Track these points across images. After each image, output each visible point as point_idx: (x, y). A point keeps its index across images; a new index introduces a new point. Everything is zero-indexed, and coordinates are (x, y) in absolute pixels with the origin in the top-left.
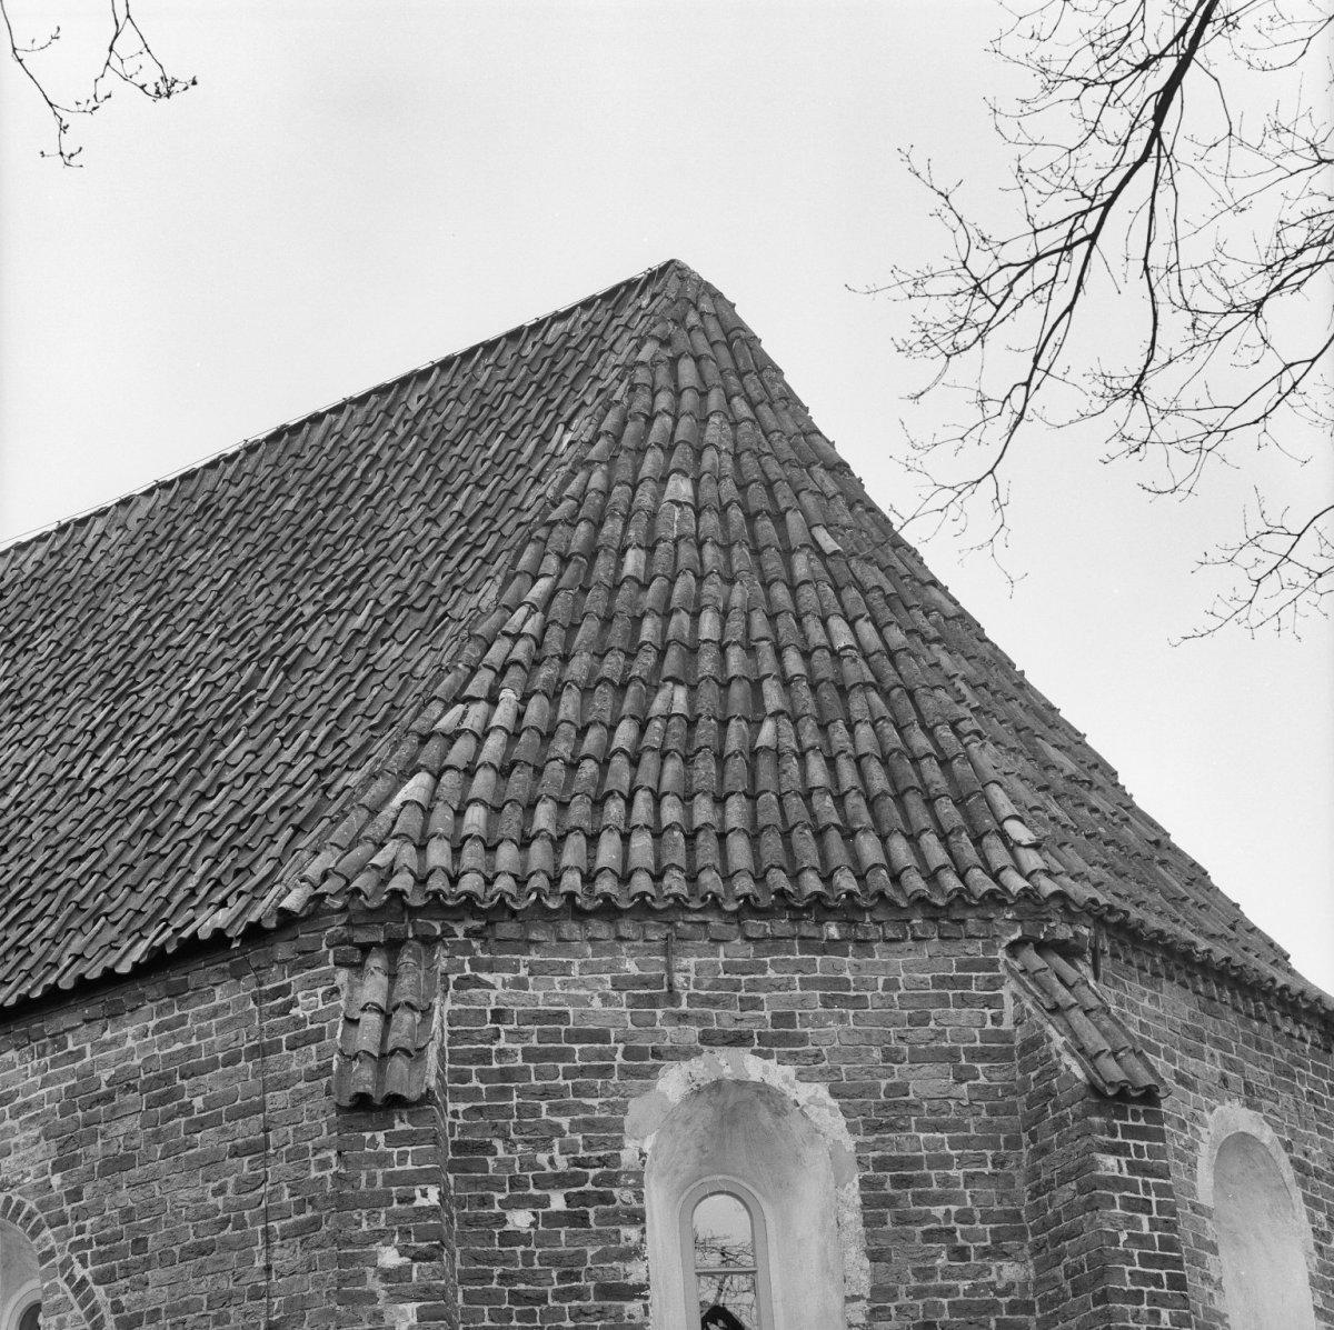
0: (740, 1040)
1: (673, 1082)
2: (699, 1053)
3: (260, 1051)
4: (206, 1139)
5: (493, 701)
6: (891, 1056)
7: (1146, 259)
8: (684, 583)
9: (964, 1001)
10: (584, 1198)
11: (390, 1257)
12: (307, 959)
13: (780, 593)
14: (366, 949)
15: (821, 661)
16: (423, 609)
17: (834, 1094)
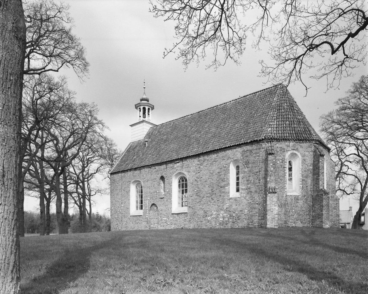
0: (294, 150)
1: (289, 153)
3: (259, 149)
4: (254, 155)
5: (274, 122)
6: (304, 151)
7: (61, 66)
8: (287, 113)
9: (310, 147)
10: (283, 161)
11: (271, 165)
12: (264, 142)
13: (294, 113)
14: (268, 142)
15: (298, 119)
16: (352, 130)
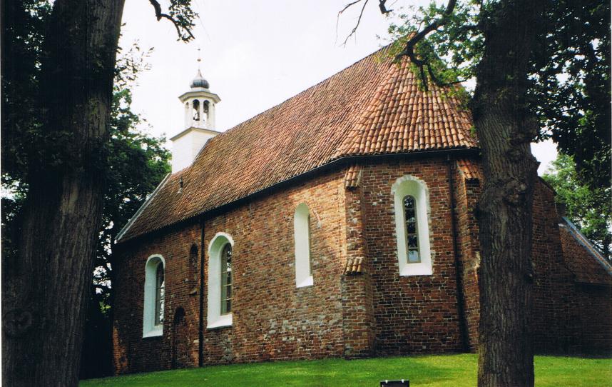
2: (402, 176)
17: (425, 181)
